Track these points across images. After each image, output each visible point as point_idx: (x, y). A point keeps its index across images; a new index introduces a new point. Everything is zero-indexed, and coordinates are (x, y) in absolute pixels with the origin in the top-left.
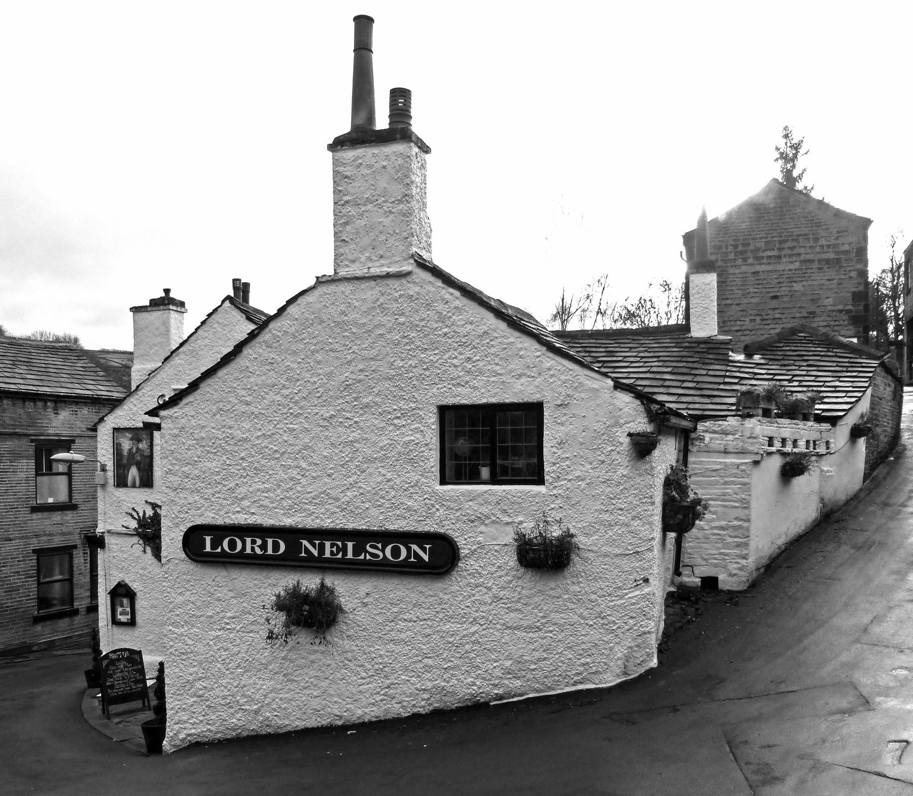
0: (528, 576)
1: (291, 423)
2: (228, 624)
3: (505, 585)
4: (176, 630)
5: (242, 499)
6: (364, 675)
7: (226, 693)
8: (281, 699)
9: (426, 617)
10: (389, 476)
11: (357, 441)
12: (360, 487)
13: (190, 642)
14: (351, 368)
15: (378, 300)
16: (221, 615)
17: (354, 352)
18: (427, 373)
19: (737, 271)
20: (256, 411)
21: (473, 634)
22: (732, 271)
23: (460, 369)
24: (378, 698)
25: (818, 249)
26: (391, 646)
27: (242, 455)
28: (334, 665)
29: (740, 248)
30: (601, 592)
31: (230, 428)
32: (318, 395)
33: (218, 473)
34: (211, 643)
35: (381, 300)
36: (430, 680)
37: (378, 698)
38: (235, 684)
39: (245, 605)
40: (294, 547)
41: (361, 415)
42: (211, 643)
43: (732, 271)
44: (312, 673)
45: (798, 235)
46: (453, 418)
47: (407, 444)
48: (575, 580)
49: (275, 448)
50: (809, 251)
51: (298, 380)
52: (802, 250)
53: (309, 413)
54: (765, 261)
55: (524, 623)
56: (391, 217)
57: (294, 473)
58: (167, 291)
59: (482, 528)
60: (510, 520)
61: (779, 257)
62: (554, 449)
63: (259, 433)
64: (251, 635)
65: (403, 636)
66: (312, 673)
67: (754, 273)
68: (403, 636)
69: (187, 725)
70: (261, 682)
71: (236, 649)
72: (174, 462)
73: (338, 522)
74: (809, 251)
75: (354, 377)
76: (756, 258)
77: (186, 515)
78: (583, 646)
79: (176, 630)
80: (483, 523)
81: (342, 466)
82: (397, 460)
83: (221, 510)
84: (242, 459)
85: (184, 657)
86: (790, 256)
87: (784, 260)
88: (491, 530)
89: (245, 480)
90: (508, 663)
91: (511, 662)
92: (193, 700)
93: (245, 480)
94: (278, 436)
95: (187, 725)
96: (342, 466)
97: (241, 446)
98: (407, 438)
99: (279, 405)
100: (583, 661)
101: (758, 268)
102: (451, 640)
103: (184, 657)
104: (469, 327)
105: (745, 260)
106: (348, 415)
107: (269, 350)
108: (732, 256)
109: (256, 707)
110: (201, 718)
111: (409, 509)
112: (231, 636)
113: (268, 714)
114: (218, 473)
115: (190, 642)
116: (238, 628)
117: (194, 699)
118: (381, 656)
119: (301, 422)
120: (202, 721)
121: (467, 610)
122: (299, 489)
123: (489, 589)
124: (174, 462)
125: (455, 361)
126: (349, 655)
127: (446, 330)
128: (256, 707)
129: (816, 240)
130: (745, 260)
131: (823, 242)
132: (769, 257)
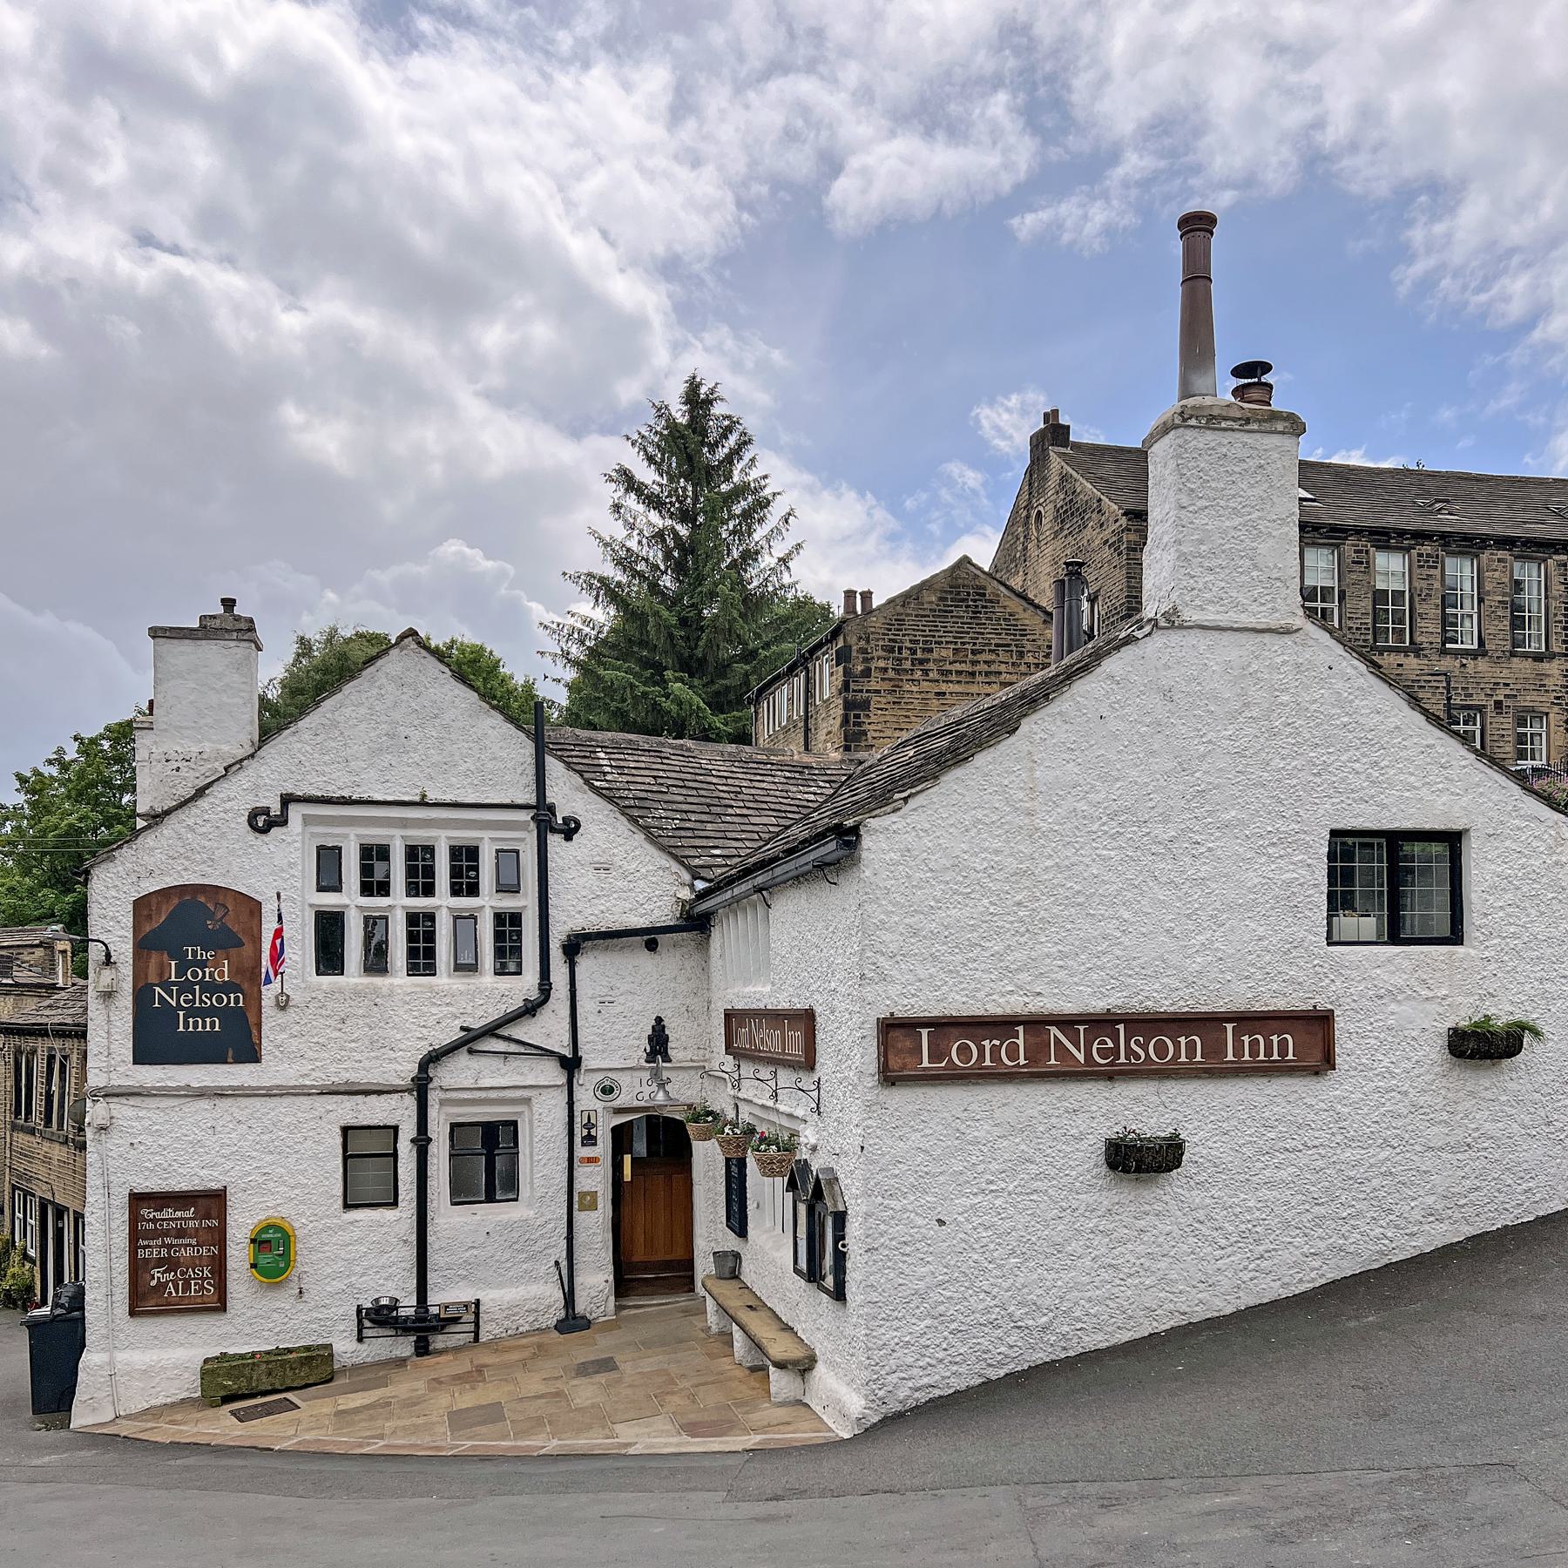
0: (1455, 1074)
1: (1105, 848)
2: (991, 1182)
3: (1426, 1087)
4: (893, 1203)
5: (1019, 970)
6: (1223, 1242)
7: (989, 1302)
8: (1090, 1300)
9: (1316, 1143)
10: (1261, 931)
11: (1212, 878)
12: (1217, 950)
13: (920, 1221)
14: (1205, 767)
15: (1249, 665)
16: (980, 1168)
17: (1210, 742)
18: (1318, 780)
19: (915, 689)
20: (1044, 826)
21: (1383, 1162)
22: (907, 687)
23: (1363, 777)
24: (1246, 1276)
25: (1023, 668)
26: (1264, 1193)
27: (1019, 898)
28: (1176, 1232)
29: (919, 655)
30: (1546, 1090)
31: (997, 852)
32: (1150, 804)
33: (974, 928)
34: (960, 1218)
35: (1255, 667)
36: (1322, 1239)
37: (1246, 1276)
38: (1006, 1285)
39: (1023, 1147)
40: (1036, 1052)
41: (1218, 839)
42: (960, 1218)
43: (907, 687)
44: (1141, 1249)
45: (997, 645)
46: (1346, 847)
47: (1289, 883)
48: (1514, 1075)
49: (1077, 888)
50: (1011, 669)
51: (1117, 780)
52: (1003, 668)
53: (1135, 833)
54: (954, 678)
55: (1452, 1140)
56: (1271, 542)
57: (1111, 927)
58: (229, 604)
59: (1393, 1007)
60: (1431, 994)
61: (973, 674)
62: (1485, 895)
63: (1049, 863)
64: (1034, 1197)
65: (1283, 1174)
66: (1141, 1249)
67: (938, 694)
68: (1283, 1174)
69: (915, 1371)
70: (1053, 1275)
71: (1008, 1224)
72: (890, 908)
73: (1182, 1003)
74: (1011, 669)
75: (1207, 778)
76: (943, 673)
77: (912, 1001)
78: (1525, 1166)
79: (893, 1203)
80: (1395, 1000)
81: (1188, 916)
82: (1273, 908)
83: (978, 990)
84: (1019, 904)
85: (908, 1249)
86: (987, 674)
87: (979, 679)
88: (1406, 1009)
89: (1022, 940)
90: (1430, 1200)
91: (1433, 1198)
92: (923, 1325)
93: (1022, 940)
94: (1082, 867)
95: (915, 1371)
96: (1188, 916)
97: (1017, 882)
98: (1288, 875)
99: (1085, 818)
100: (1524, 1186)
101: (944, 687)
102: (1352, 1174)
103: (908, 1249)
104: (1378, 718)
105: (926, 672)
106: (1198, 838)
107: (1067, 726)
108: (907, 665)
109: (1045, 1319)
110: (941, 1355)
111: (1292, 981)
112: (998, 1202)
113: (1066, 1328)
114: (974, 928)
115: (920, 1221)
116: (1011, 1188)
117: (928, 1322)
118: (1249, 1210)
119: (1121, 847)
120: (941, 1361)
121: (1374, 1127)
122: (1119, 953)
123: (1406, 1093)
124: (890, 908)
125: (1357, 765)
126: (1201, 1215)
127: (1345, 719)
128: (1045, 1319)
129: (1021, 655)
130: (926, 672)
131: (1029, 659)
132: (959, 673)
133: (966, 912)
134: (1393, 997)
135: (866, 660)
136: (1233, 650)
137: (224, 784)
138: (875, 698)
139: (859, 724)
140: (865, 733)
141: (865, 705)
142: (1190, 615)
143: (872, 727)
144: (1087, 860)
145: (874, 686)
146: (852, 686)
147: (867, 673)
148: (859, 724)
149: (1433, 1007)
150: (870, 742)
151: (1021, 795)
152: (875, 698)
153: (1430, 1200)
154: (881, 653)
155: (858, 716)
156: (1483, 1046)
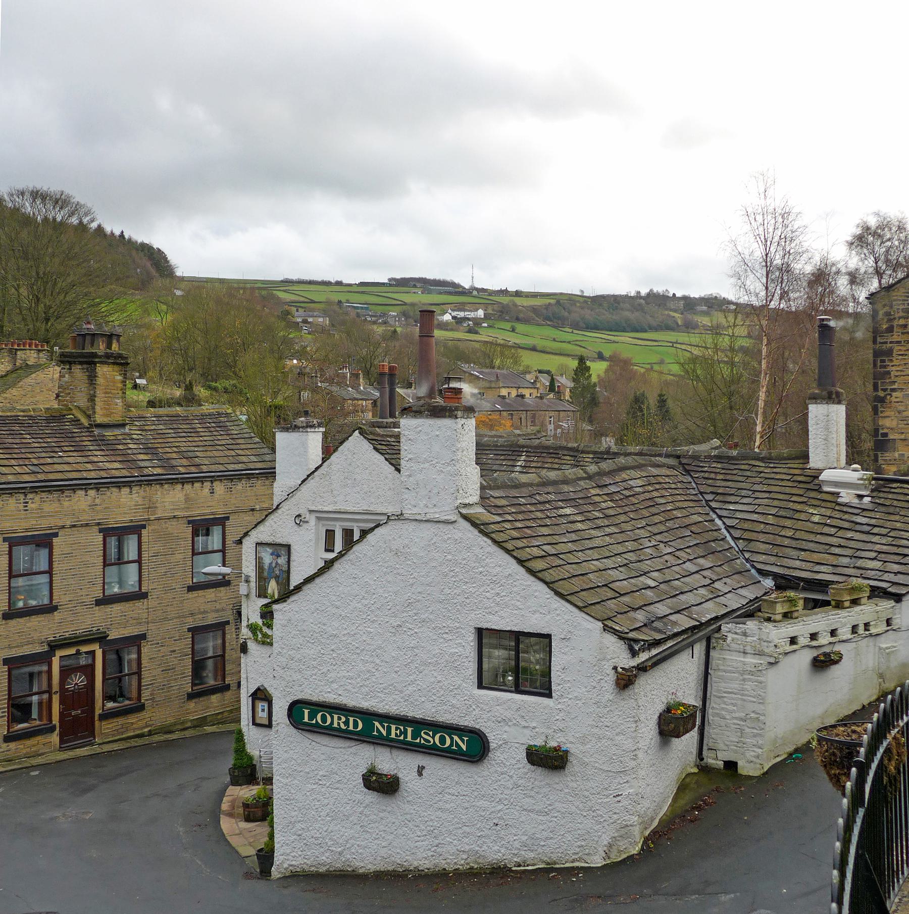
4: (283, 780)
8: (358, 846)
10: (439, 678)
11: (416, 647)
18: (468, 601)
21: (499, 811)
26: (439, 813)
33: (315, 659)
48: (573, 778)
55: (536, 808)
56: (442, 475)
59: (507, 728)
60: (526, 725)
63: (346, 632)
68: (448, 806)
71: (326, 801)
81: (406, 666)
90: (524, 838)
91: (526, 837)
94: (359, 636)
104: (498, 569)
106: (410, 626)
112: (323, 790)
113: (348, 856)
114: (315, 659)
118: (431, 820)
123: (511, 777)
125: (488, 594)
133: (312, 652)
134: (511, 720)
135: (890, 320)
136: (428, 531)
137: (287, 503)
138: (896, 348)
139: (885, 367)
140: (889, 373)
141: (890, 353)
142: (407, 513)
143: (894, 368)
144: (361, 633)
145: (895, 338)
146: (879, 339)
147: (890, 330)
148: (885, 367)
149: (527, 732)
150: (893, 379)
151: (334, 598)
152: (896, 348)
153: (524, 838)
154: (901, 314)
155: (883, 361)
156: (549, 759)
